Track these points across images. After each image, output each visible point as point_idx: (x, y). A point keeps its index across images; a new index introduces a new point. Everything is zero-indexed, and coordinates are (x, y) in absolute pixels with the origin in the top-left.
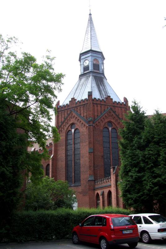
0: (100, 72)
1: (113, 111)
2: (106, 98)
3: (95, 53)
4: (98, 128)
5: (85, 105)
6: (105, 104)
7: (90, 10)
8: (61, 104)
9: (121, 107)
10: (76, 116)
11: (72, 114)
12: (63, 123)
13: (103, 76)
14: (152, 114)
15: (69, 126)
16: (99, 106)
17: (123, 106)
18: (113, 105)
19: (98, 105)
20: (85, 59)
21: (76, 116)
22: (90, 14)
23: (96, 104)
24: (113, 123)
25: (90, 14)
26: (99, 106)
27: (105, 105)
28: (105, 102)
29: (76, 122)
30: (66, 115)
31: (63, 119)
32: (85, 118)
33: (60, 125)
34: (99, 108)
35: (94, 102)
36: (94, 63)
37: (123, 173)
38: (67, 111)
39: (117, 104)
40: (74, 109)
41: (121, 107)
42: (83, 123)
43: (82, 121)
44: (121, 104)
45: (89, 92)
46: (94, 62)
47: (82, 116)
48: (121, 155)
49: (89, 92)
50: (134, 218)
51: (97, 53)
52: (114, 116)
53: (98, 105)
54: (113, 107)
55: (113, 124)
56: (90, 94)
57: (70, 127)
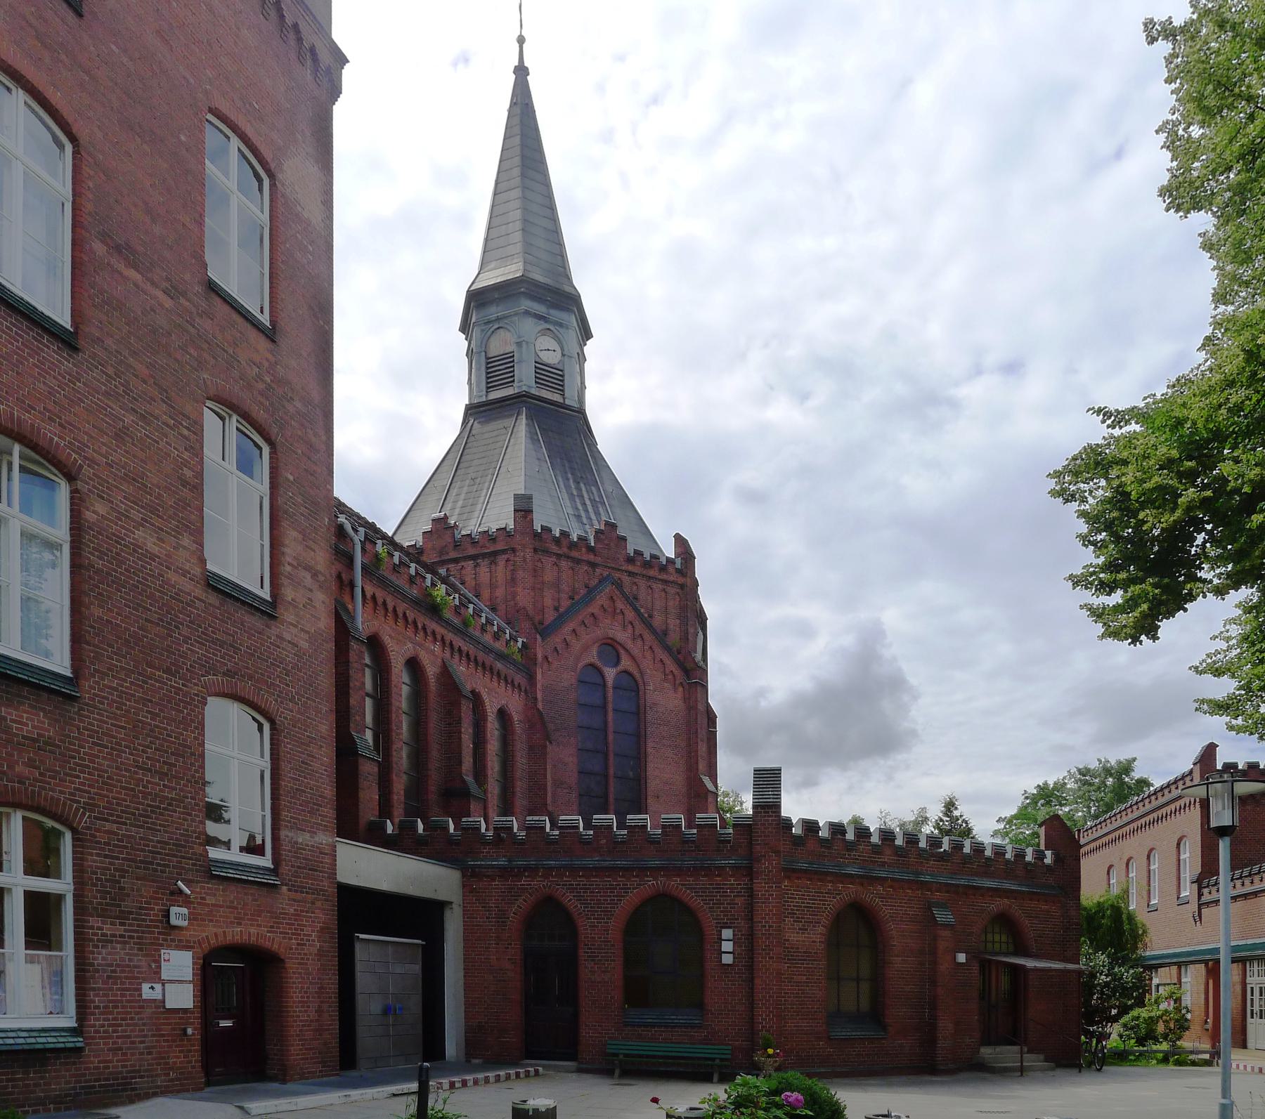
0: (567, 402)
2: (598, 533)
6: (591, 557)
7: (521, 40)
14: (1204, 275)
17: (582, 554)
22: (521, 71)
24: (626, 650)
25: (521, 71)
28: (591, 549)
33: (547, 622)
37: (1218, 229)
39: (647, 565)
44: (663, 569)
45: (517, 497)
48: (1123, 430)
49: (517, 497)
52: (630, 615)
56: (524, 509)
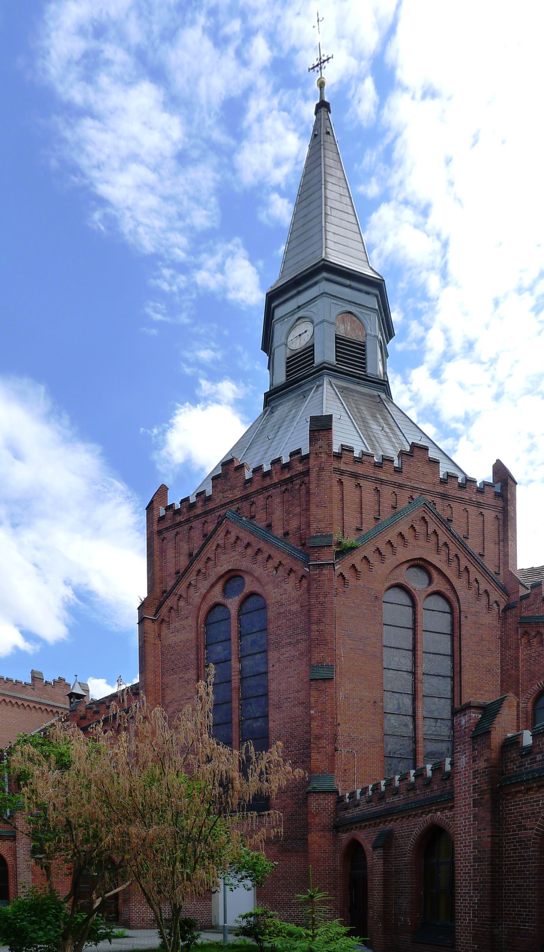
1: (437, 516)
3: (348, 282)
4: (360, 582)
5: (290, 480)
6: (397, 479)
8: (174, 499)
9: (479, 505)
10: (246, 538)
11: (228, 532)
12: (180, 575)
13: (383, 396)
15: (213, 586)
16: (368, 486)
18: (440, 489)
19: (362, 482)
20: (296, 316)
21: (246, 538)
23: (355, 476)
26: (368, 486)
27: (400, 486)
29: (245, 564)
30: (198, 542)
31: (184, 561)
32: (293, 540)
34: (369, 496)
35: (343, 467)
36: (341, 332)
38: (200, 526)
40: (234, 508)
41: (479, 505)
42: (280, 563)
43: (278, 557)
46: (342, 327)
47: (279, 531)
50: (203, 947)
51: (354, 284)
53: (362, 482)
54: (437, 500)
55: (435, 574)
57: (218, 588)
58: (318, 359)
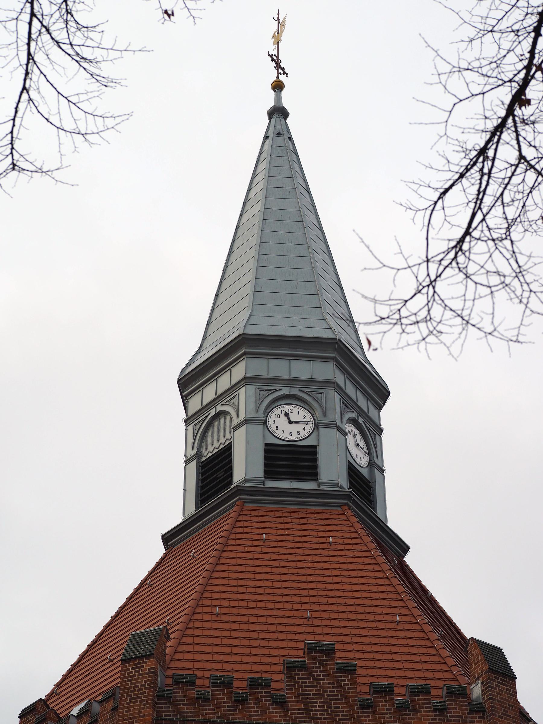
58: (239, 474)
